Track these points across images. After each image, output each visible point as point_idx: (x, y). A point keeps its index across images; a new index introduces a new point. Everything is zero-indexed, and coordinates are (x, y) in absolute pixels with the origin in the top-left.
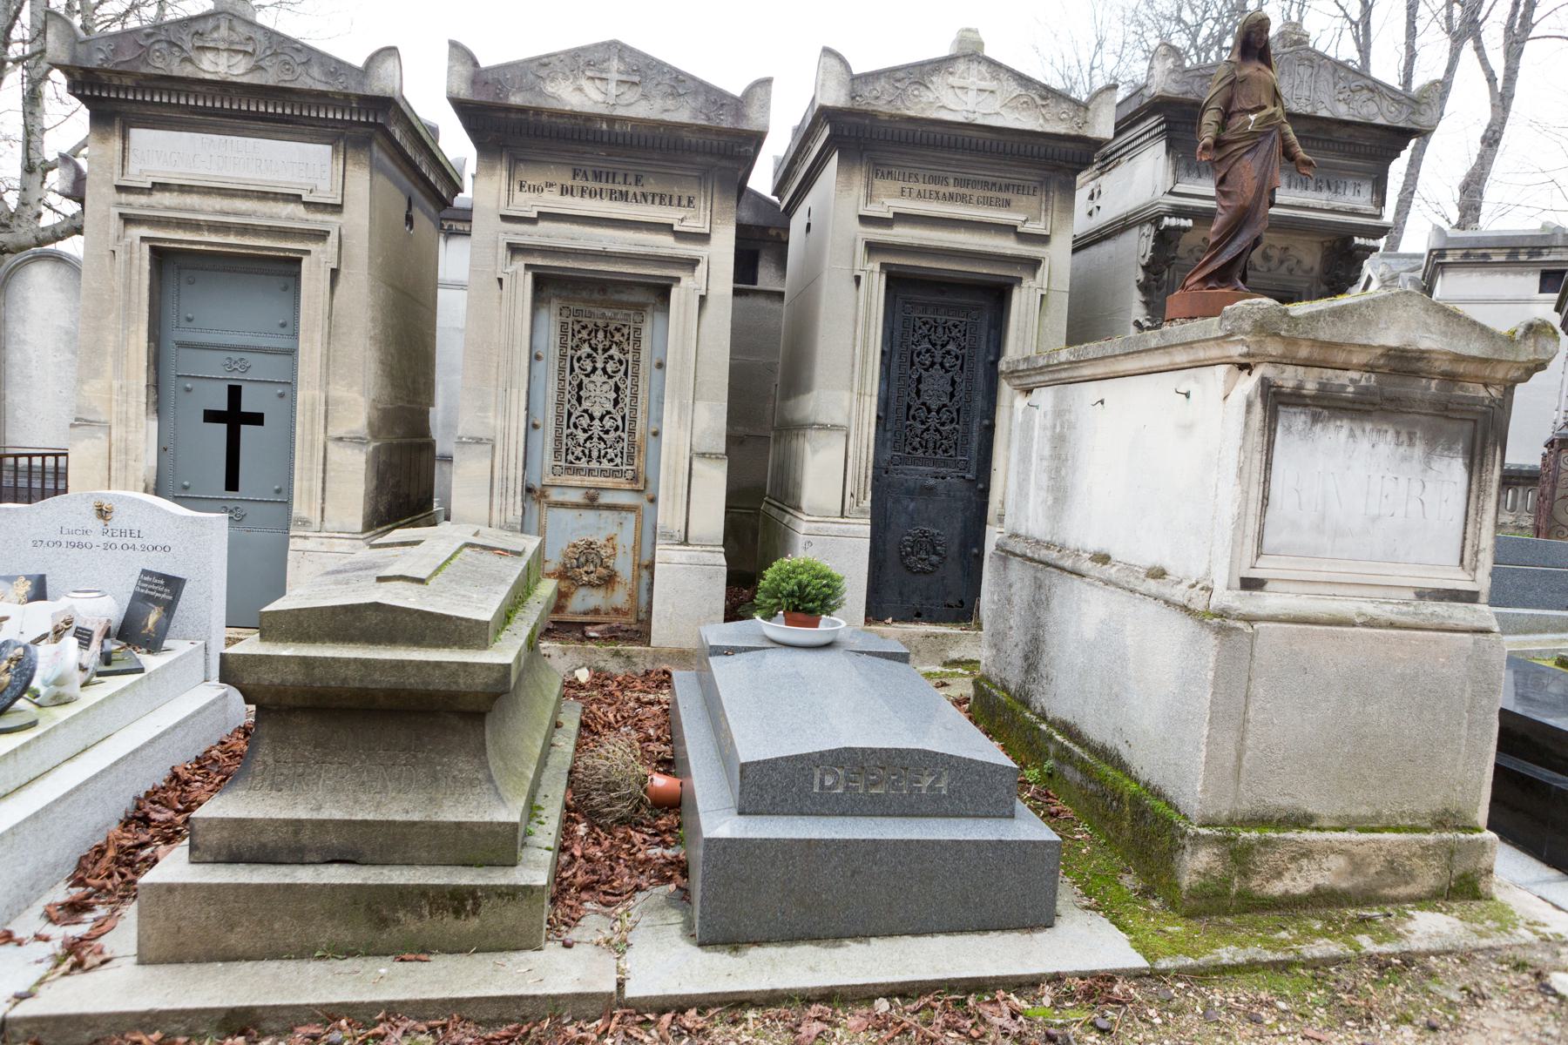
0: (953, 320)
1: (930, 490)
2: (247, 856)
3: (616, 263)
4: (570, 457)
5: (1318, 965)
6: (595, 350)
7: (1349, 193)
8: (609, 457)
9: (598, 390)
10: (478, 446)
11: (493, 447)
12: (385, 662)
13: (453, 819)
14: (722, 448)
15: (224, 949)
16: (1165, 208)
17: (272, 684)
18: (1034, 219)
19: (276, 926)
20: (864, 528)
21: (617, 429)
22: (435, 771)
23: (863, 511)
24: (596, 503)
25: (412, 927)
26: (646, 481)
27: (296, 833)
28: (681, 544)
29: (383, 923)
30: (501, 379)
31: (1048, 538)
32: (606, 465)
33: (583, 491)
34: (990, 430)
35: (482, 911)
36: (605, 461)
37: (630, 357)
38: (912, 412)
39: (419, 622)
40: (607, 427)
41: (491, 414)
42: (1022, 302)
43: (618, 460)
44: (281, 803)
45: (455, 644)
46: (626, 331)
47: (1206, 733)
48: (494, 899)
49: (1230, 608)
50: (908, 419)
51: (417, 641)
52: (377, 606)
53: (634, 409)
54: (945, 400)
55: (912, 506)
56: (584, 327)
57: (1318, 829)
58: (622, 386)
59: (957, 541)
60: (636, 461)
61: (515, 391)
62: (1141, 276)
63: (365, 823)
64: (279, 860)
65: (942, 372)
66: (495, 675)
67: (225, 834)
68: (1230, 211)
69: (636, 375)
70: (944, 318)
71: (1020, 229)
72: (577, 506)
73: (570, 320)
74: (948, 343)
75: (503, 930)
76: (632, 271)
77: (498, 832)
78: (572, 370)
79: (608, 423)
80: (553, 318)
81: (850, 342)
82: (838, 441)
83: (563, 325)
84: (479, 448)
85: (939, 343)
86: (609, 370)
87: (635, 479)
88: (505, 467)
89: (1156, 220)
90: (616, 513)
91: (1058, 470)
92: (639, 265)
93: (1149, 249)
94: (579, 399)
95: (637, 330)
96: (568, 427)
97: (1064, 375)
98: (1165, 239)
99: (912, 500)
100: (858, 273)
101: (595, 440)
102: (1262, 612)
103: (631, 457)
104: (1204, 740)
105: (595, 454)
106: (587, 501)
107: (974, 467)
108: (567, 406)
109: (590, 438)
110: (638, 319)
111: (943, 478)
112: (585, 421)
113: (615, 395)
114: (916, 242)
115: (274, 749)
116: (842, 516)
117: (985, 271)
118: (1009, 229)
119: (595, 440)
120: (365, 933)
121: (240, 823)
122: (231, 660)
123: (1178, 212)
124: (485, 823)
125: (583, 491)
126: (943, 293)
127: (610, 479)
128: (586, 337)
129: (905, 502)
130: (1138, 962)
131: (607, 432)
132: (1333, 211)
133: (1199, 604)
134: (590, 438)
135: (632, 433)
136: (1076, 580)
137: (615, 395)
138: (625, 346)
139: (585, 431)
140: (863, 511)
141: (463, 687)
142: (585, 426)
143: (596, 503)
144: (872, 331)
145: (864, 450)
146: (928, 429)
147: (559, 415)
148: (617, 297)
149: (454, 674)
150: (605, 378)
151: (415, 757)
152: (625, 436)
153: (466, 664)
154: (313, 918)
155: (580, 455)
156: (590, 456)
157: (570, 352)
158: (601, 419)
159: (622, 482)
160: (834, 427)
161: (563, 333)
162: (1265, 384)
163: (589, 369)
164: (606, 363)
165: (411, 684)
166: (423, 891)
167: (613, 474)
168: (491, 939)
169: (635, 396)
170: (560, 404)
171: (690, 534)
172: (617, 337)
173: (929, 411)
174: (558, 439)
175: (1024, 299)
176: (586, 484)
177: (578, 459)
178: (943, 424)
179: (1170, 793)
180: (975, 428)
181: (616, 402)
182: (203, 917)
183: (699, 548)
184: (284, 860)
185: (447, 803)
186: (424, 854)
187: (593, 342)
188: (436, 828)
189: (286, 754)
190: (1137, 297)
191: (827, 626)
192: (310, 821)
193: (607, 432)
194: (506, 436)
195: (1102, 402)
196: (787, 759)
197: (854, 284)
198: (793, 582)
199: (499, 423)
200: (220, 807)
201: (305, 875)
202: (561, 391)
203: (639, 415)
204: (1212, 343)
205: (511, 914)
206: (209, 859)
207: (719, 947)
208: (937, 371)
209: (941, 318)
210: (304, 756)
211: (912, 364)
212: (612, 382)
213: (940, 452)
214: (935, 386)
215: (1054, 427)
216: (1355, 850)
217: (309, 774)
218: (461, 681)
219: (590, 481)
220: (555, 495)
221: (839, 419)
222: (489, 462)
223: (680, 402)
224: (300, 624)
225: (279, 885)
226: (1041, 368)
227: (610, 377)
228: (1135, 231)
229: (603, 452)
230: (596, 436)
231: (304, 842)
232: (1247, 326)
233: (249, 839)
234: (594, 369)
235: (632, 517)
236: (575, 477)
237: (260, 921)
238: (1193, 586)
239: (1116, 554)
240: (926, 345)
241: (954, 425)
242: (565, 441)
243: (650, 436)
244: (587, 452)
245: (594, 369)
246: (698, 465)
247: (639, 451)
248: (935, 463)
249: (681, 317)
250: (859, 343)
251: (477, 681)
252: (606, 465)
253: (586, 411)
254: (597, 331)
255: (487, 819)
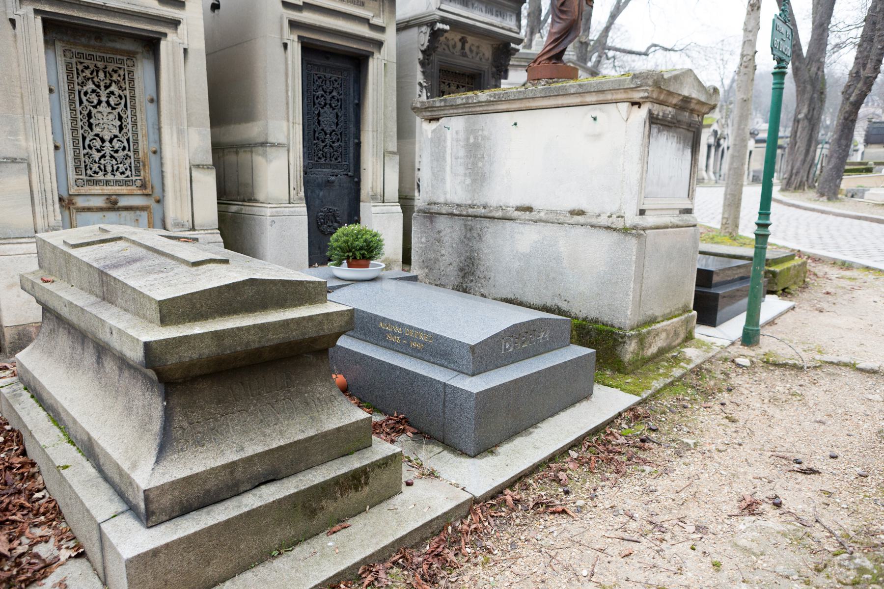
0: (334, 77)
1: (329, 183)
2: (196, 504)
3: (115, 17)
4: (89, 172)
5: (680, 379)
6: (98, 86)
7: (508, 19)
8: (120, 170)
9: (105, 119)
10: (13, 165)
11: (29, 165)
12: (275, 323)
13: (335, 427)
14: (209, 160)
15: (204, 582)
16: (437, 17)
17: (192, 360)
18: (377, 16)
19: (242, 547)
20: (303, 209)
21: (124, 149)
22: (305, 397)
23: (300, 199)
24: (116, 206)
25: (331, 509)
26: (152, 188)
27: (232, 473)
28: (190, 230)
29: (313, 513)
30: (27, 108)
31: (470, 202)
32: (119, 176)
33: (104, 198)
34: (358, 146)
35: (370, 481)
36: (118, 173)
37: (127, 93)
38: (317, 135)
39: (282, 289)
40: (116, 148)
41: (21, 137)
42: (374, 66)
43: (128, 173)
44: (211, 454)
45: (306, 302)
46: (121, 73)
47: (632, 286)
48: (377, 470)
49: (638, 224)
50: (315, 140)
51: (281, 304)
52: (252, 281)
53: (135, 134)
54: (334, 127)
55: (321, 193)
56: (87, 68)
57: (658, 322)
58: (124, 116)
59: (346, 213)
60: (142, 173)
61: (41, 118)
62: (421, 56)
63: (280, 448)
64: (222, 497)
65: (331, 110)
66: (346, 318)
67: (177, 493)
68: (568, 21)
69: (134, 107)
70: (330, 75)
71: (371, 22)
72: (101, 209)
73: (74, 60)
74: (332, 91)
75: (382, 488)
76: (129, 25)
77: (361, 427)
78: (81, 102)
79: (117, 144)
80: (59, 59)
81: (284, 88)
82: (283, 153)
83: (68, 66)
84: (16, 166)
85: (328, 91)
86: (112, 103)
87: (143, 186)
88: (42, 182)
89: (431, 24)
90: (132, 212)
91: (474, 164)
92: (134, 20)
93: (427, 41)
94: (90, 126)
95: (130, 72)
96: (84, 148)
97: (478, 109)
98: (435, 35)
99: (321, 190)
100: (286, 41)
101: (108, 157)
102: (649, 225)
103: (138, 170)
104: (632, 290)
105: (109, 169)
106: (109, 205)
107: (352, 168)
108: (81, 132)
109: (104, 156)
110: (130, 63)
111: (337, 176)
112: (97, 143)
113: (119, 123)
114: (318, 23)
115: (186, 414)
116: (290, 203)
117: (355, 46)
118: (365, 21)
119: (108, 157)
120: (302, 525)
121: (187, 480)
122: (155, 346)
123: (444, 21)
124: (354, 423)
125: (104, 198)
126: (328, 58)
127: (124, 187)
128: (89, 76)
129: (317, 192)
130: (637, 399)
131: (117, 151)
132: (503, 28)
133: (619, 224)
134: (104, 156)
135: (136, 152)
136: (508, 224)
137: (119, 123)
138: (123, 84)
139: (98, 151)
140: (300, 199)
141: (327, 332)
142: (98, 147)
143: (116, 206)
144: (296, 80)
145: (298, 159)
146: (326, 146)
147: (74, 139)
148: (110, 44)
149: (321, 323)
150: (109, 110)
151: (289, 391)
152: (131, 154)
153: (328, 314)
154: (267, 530)
155: (97, 170)
156: (105, 171)
157: (77, 88)
158: (111, 141)
159: (133, 189)
160: (280, 145)
161: (69, 72)
162: (650, 113)
163: (96, 102)
164: (109, 97)
165: (294, 337)
166: (336, 482)
167: (126, 183)
168: (375, 497)
169: (135, 124)
170: (74, 129)
171: (196, 223)
172: (115, 77)
173: (326, 134)
174: (76, 158)
175: (375, 64)
176: (106, 192)
177: (97, 173)
178: (333, 142)
179: (606, 319)
180: (351, 145)
181: (121, 128)
182: (185, 563)
183: (202, 232)
184: (225, 496)
185: (324, 417)
186: (319, 457)
187: (96, 80)
188: (325, 436)
189: (197, 415)
190: (419, 69)
191: (376, 266)
192: (242, 460)
193: (117, 151)
194: (39, 156)
195: (515, 124)
196: (491, 337)
197: (283, 49)
198: (362, 240)
199: (32, 145)
200: (164, 474)
201: (252, 501)
202: (74, 119)
203: (140, 138)
204: (622, 91)
205: (385, 476)
206: (165, 518)
207: (484, 454)
208: (327, 109)
209: (328, 75)
210: (211, 413)
211: (314, 104)
212: (115, 112)
213: (333, 159)
214: (328, 116)
215: (468, 139)
216: (668, 328)
217: (220, 426)
218: (325, 327)
219: (108, 190)
220: (81, 202)
221: (282, 139)
222: (26, 178)
223: (177, 128)
224: (193, 306)
225: (241, 515)
226: (458, 105)
227: (113, 109)
228: (415, 31)
229: (115, 167)
230: (108, 155)
231: (238, 477)
232: (650, 82)
233: (197, 490)
234: (100, 102)
235: (144, 214)
236: (96, 187)
237: (230, 548)
238: (610, 217)
239: (535, 205)
240: (320, 93)
241: (339, 143)
242: (83, 159)
243: (151, 154)
244: (102, 167)
245: (100, 102)
246: (195, 173)
247: (144, 165)
248: (331, 166)
249: (171, 64)
250: (290, 89)
251: (335, 325)
252: (119, 176)
253: (97, 135)
254: (97, 72)
255: (354, 420)
